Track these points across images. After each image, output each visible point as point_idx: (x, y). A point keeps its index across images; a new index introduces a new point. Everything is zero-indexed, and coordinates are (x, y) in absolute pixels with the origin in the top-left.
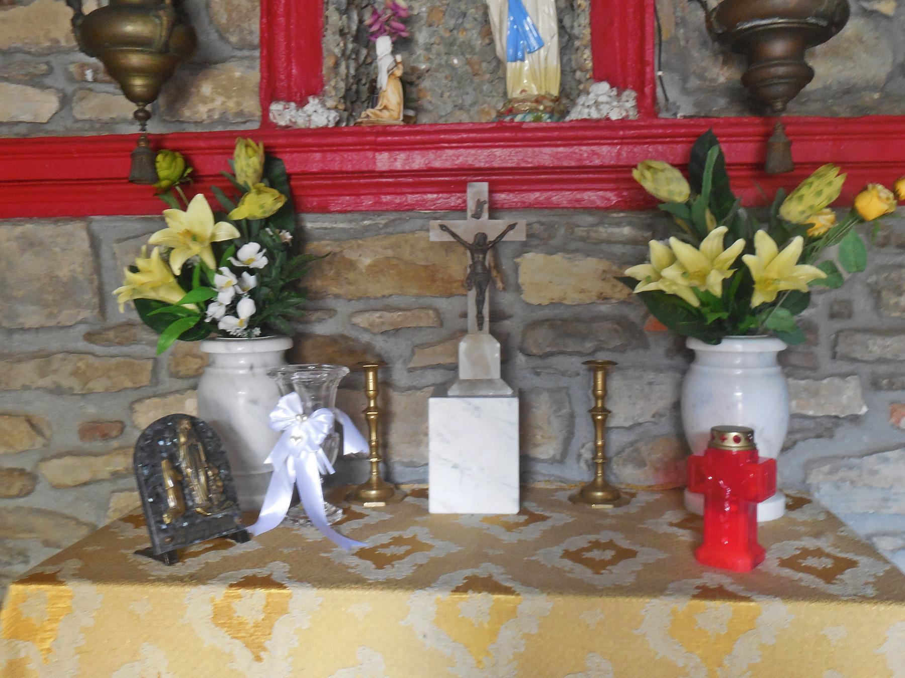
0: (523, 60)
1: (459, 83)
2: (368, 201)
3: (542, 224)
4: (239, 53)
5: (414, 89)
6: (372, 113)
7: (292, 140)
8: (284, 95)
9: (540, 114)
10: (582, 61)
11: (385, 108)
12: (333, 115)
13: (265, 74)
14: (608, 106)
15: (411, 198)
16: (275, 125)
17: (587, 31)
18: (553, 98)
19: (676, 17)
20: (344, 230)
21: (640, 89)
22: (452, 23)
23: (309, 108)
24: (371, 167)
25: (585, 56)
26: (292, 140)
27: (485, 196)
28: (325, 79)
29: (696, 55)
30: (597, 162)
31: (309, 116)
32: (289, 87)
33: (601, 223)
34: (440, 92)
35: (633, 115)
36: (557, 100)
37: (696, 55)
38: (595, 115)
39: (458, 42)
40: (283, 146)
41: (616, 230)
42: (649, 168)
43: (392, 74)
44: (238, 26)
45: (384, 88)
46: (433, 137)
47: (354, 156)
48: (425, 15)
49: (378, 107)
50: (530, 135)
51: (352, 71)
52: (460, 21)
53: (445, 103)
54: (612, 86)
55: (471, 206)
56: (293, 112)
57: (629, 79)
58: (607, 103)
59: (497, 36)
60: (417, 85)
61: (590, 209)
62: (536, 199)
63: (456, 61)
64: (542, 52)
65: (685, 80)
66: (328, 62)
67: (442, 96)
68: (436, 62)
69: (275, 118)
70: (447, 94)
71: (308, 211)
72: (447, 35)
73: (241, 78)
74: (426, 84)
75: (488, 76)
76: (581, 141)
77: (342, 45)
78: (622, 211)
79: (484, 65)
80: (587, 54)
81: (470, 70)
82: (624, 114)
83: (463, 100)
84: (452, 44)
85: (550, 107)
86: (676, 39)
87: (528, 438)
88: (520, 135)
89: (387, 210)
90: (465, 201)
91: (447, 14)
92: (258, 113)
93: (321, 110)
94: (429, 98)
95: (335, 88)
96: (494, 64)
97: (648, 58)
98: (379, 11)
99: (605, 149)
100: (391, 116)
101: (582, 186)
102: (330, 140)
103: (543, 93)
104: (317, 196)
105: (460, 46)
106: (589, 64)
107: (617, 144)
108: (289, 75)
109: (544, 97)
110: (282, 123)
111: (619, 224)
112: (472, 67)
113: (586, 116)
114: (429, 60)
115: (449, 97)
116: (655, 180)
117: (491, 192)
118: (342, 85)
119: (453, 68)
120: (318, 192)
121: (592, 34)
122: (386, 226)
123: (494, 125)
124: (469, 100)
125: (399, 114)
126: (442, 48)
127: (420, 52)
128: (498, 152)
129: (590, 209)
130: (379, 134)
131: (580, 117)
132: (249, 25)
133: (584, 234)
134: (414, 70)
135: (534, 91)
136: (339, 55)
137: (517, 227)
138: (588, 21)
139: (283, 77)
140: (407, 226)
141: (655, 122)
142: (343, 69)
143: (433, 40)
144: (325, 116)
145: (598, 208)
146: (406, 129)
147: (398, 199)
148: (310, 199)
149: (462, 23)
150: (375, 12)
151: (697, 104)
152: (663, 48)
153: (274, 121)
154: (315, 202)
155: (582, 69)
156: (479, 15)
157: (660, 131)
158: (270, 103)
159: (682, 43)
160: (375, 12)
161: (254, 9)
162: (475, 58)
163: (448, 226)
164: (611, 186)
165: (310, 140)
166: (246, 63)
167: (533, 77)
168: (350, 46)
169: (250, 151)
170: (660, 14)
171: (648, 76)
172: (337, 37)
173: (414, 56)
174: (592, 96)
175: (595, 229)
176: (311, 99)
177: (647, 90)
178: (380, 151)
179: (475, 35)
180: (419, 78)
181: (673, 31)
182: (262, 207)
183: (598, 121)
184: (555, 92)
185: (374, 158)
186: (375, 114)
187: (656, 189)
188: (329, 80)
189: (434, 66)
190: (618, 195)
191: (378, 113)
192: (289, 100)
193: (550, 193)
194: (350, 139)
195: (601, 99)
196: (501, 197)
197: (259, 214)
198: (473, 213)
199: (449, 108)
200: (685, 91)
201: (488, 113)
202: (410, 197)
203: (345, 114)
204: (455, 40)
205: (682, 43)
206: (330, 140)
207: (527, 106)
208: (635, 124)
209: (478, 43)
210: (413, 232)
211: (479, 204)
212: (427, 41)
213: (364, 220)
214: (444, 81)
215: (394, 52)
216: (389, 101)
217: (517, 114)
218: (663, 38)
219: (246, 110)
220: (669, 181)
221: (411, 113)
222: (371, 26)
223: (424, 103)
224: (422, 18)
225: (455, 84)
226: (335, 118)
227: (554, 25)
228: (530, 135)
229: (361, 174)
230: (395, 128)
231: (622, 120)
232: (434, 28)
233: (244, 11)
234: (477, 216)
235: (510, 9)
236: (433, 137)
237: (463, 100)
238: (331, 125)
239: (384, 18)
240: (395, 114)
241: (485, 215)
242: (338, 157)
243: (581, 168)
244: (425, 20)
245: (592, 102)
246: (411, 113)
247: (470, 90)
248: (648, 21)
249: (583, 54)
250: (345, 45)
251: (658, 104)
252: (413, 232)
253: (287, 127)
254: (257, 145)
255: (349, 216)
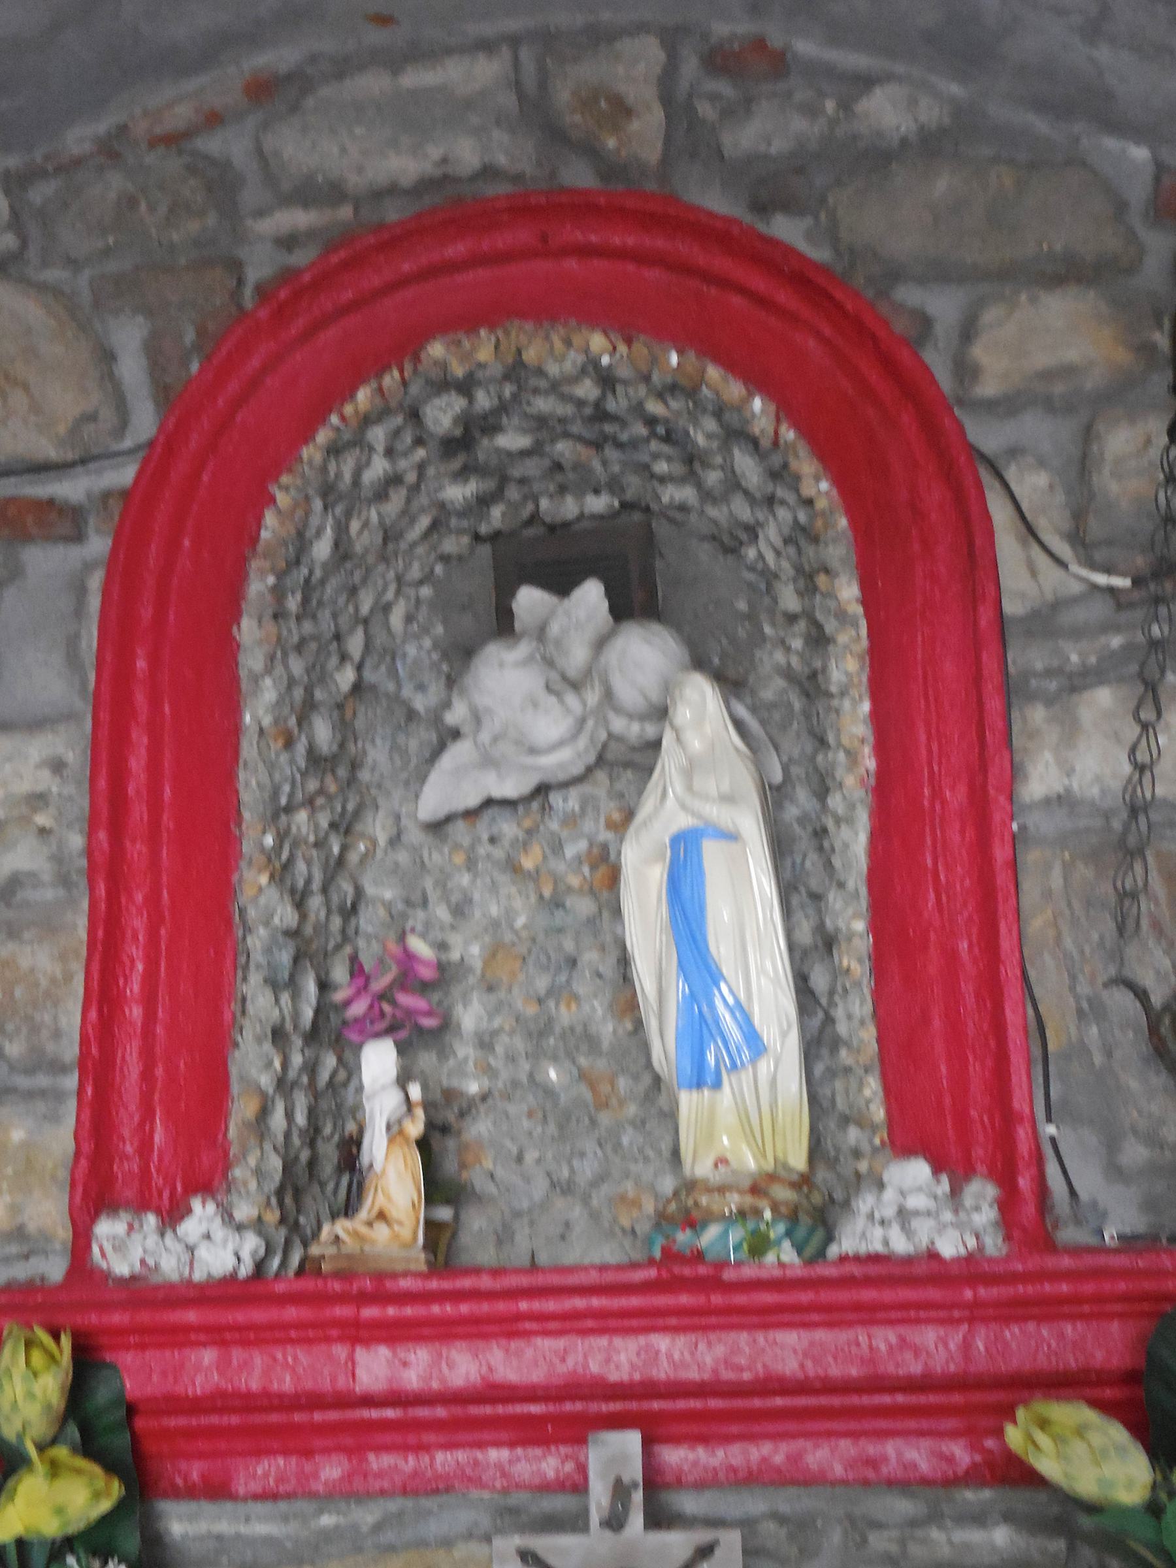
0: (717, 1085)
1: (561, 1127)
2: (331, 1470)
3: (780, 1519)
4: (23, 1082)
5: (451, 1143)
6: (346, 1231)
7: (145, 1317)
8: (129, 1193)
9: (719, 460)
10: (862, 1103)
11: (382, 1216)
12: (251, 1244)
13: (87, 1148)
14: (930, 1223)
15: (444, 1460)
16: (106, 1276)
17: (869, 1035)
18: (795, 1177)
19: (1077, 998)
20: (269, 1541)
21: (1005, 1178)
22: (542, 983)
23: (190, 1227)
24: (342, 1383)
25: (867, 1092)
26: (145, 1317)
27: (635, 1471)
28: (234, 1150)
29: (1134, 1084)
30: (915, 1368)
31: (191, 1249)
32: (145, 1172)
33: (934, 1517)
34: (515, 1151)
35: (994, 1245)
36: (804, 1182)
37: (1134, 1084)
38: (900, 1245)
39: (558, 1030)
40: (121, 1331)
41: (974, 1536)
42: (1044, 1424)
43: (401, 1132)
44: (29, 1019)
45: (378, 1167)
46: (502, 1307)
47: (302, 1357)
48: (478, 965)
49: (364, 1214)
50: (740, 1299)
51: (301, 1119)
52: (563, 978)
53: (527, 1180)
54: (937, 1170)
55: (599, 1495)
56: (152, 1240)
57: (978, 1152)
58: (929, 1213)
59: (652, 1025)
60: (459, 1133)
61: (905, 1483)
62: (764, 1460)
63: (553, 1075)
64: (765, 1067)
65: (1112, 1145)
66: (242, 1109)
67: (520, 1159)
68: (505, 1075)
69: (103, 1255)
70: (531, 1156)
71: (176, 1494)
72: (531, 1010)
73: (26, 1145)
74: (480, 1128)
75: (632, 1110)
76: (869, 1314)
77: (277, 1064)
78: (982, 1483)
79: (623, 1083)
80: (873, 1086)
81: (588, 1096)
82: (972, 1243)
83: (572, 1171)
84: (543, 1034)
85: (787, 1203)
86: (1082, 1049)
87: (729, 1519)
88: (717, 1299)
89: (383, 1492)
90: (582, 1469)
91: (531, 961)
92: (63, 1233)
93: (219, 1231)
94: (488, 1164)
95: (259, 1173)
96: (647, 1080)
97: (1019, 1103)
98: (368, 966)
99: (928, 1336)
100: (396, 1236)
101: (883, 1424)
102: (239, 1316)
103: (769, 1166)
104: (201, 1455)
105: (563, 1036)
106: (878, 1113)
107: (959, 1321)
108: (145, 1147)
109: (772, 1177)
110: (122, 1268)
111: (979, 1519)
112: (593, 1087)
113: (877, 1247)
114: (489, 1071)
115: (539, 1161)
116: (1061, 1456)
117: (648, 1443)
118: (275, 1163)
119: (549, 1092)
120: (202, 1445)
121: (880, 1040)
122: (378, 1528)
123: (652, 1273)
124: (587, 1169)
125: (415, 1233)
126: (519, 1044)
127: (465, 1051)
128: (662, 1342)
129: (905, 1483)
130: (364, 1298)
131: (863, 1249)
132: (55, 1018)
133: (894, 1548)
134: (450, 1095)
135: (749, 1162)
136: (271, 1091)
137: (718, 1552)
138: (869, 1007)
139: (129, 1149)
140: (434, 1528)
141: (1051, 1262)
142: (278, 1120)
143: (497, 1023)
144: (230, 1247)
145: (925, 1482)
146: (434, 1284)
147: (410, 1463)
148: (183, 1465)
149: (568, 982)
150: (356, 969)
151: (1150, 1205)
152: (1052, 1069)
153: (104, 1265)
154: (195, 1471)
155: (861, 1120)
156: (608, 967)
157: (1065, 1288)
158: (94, 1218)
159: (1098, 1059)
160: (356, 969)
161: (68, 977)
162: (601, 1064)
163: (542, 1553)
164: (950, 1423)
165: (191, 1316)
166: (41, 1106)
167: (747, 1130)
168: (297, 1060)
169: (37, 1357)
170: (1038, 992)
171: (1024, 1147)
172: (268, 1046)
173: (452, 1062)
174: (889, 1195)
175: (919, 1533)
176: (196, 1204)
177: (1024, 1183)
178: (367, 1342)
179: (600, 1012)
180: (462, 1114)
181: (1073, 1030)
182: (59, 1511)
183: (908, 1260)
184: (798, 1160)
185: (352, 1359)
186: (356, 1234)
187: (1066, 1475)
188: (244, 1155)
189: (500, 1085)
190: (974, 1447)
191: (363, 1230)
192: (142, 1205)
193: (800, 1443)
194: (291, 1313)
195: (916, 1202)
196: (673, 1456)
197: (51, 1528)
198: (606, 1513)
199: (540, 1187)
200: (1115, 1172)
201: (636, 1203)
202: (441, 1457)
203: (281, 1235)
204: (550, 1021)
205: (1098, 1059)
206: (239, 1316)
207: (734, 1201)
208: (1000, 1269)
209: (607, 1030)
210: (447, 1543)
211: (620, 1491)
212: (484, 1025)
213: (320, 1512)
214: (526, 1123)
215: (403, 1081)
216: (389, 1198)
217: (705, 1224)
218: (1051, 1047)
219: (32, 1227)
220: (1098, 1457)
221: (444, 1213)
222: (347, 1003)
223: (477, 1178)
224: (470, 970)
225: (552, 1129)
226: (254, 1253)
227: (788, 1003)
228: (740, 1299)
229: (315, 1401)
230: (405, 1284)
231: (969, 1259)
232: (502, 994)
233: (44, 983)
234: (615, 1522)
235: (681, 966)
236: (502, 1307)
237: (572, 1171)
238: (245, 1270)
239: (378, 985)
240: (405, 1233)
241: (636, 1520)
242: (258, 1360)
243: (876, 1384)
244: (478, 972)
245: (890, 1212)
246: (444, 1213)
247: (589, 1145)
248: (1011, 1017)
249: (861, 1085)
250: (285, 1065)
251: (1053, 1207)
252: (447, 1543)
253: (133, 1278)
254: (56, 1337)
255: (283, 1506)
